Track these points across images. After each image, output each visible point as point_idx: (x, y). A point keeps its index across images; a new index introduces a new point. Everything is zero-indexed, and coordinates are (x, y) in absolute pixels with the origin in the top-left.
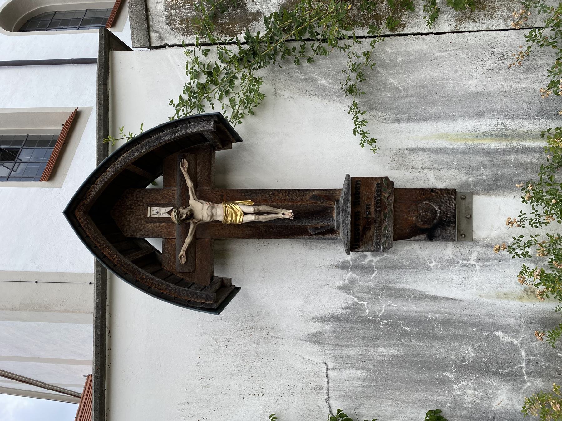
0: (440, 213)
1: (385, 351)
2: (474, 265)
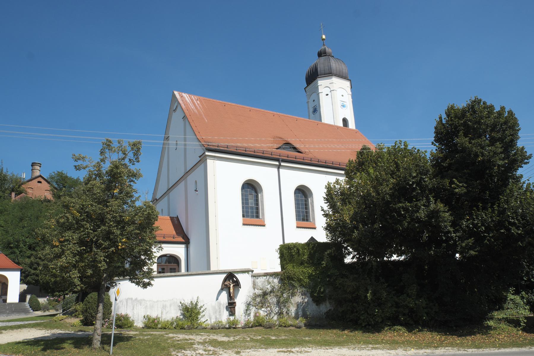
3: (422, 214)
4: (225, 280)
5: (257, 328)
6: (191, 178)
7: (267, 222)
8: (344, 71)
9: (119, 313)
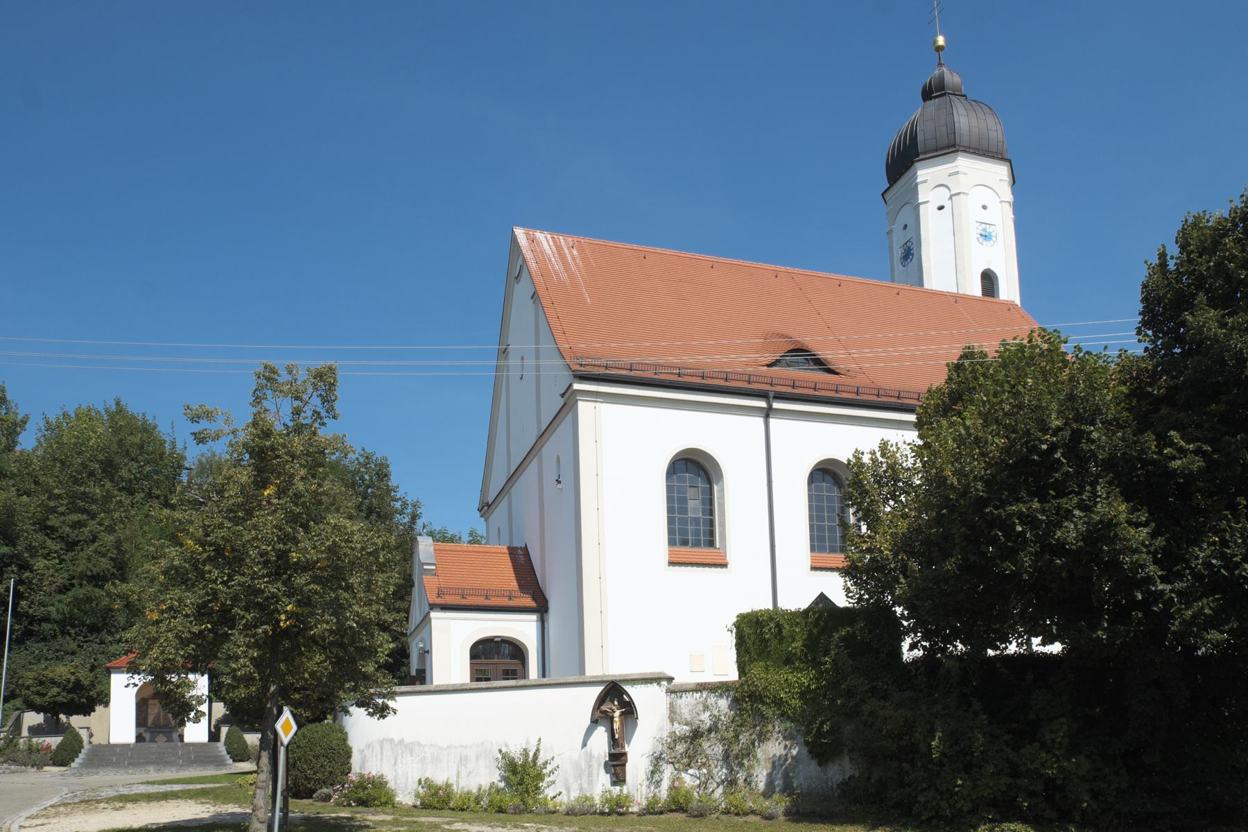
3: (1070, 532)
4: (601, 700)
5: (676, 815)
6: (550, 450)
7: (730, 558)
8: (993, 134)
9: (366, 772)
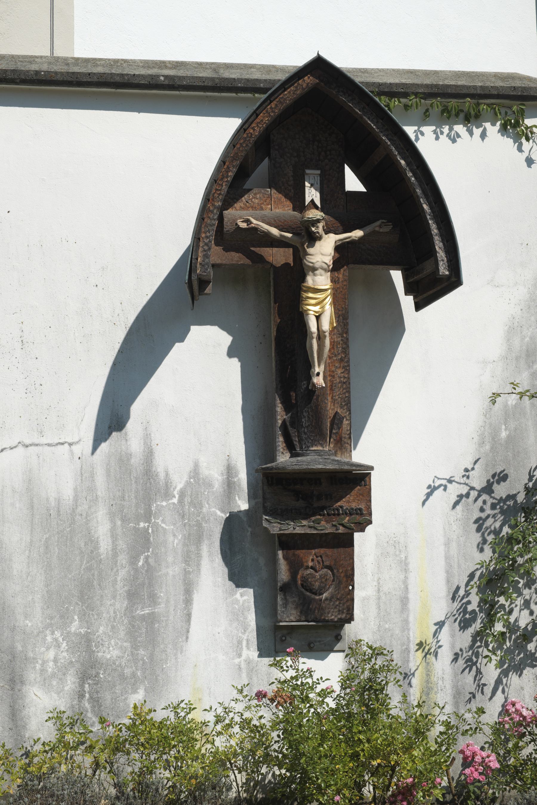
0: (321, 600)
1: (102, 528)
2: (240, 656)
4: (232, 179)
